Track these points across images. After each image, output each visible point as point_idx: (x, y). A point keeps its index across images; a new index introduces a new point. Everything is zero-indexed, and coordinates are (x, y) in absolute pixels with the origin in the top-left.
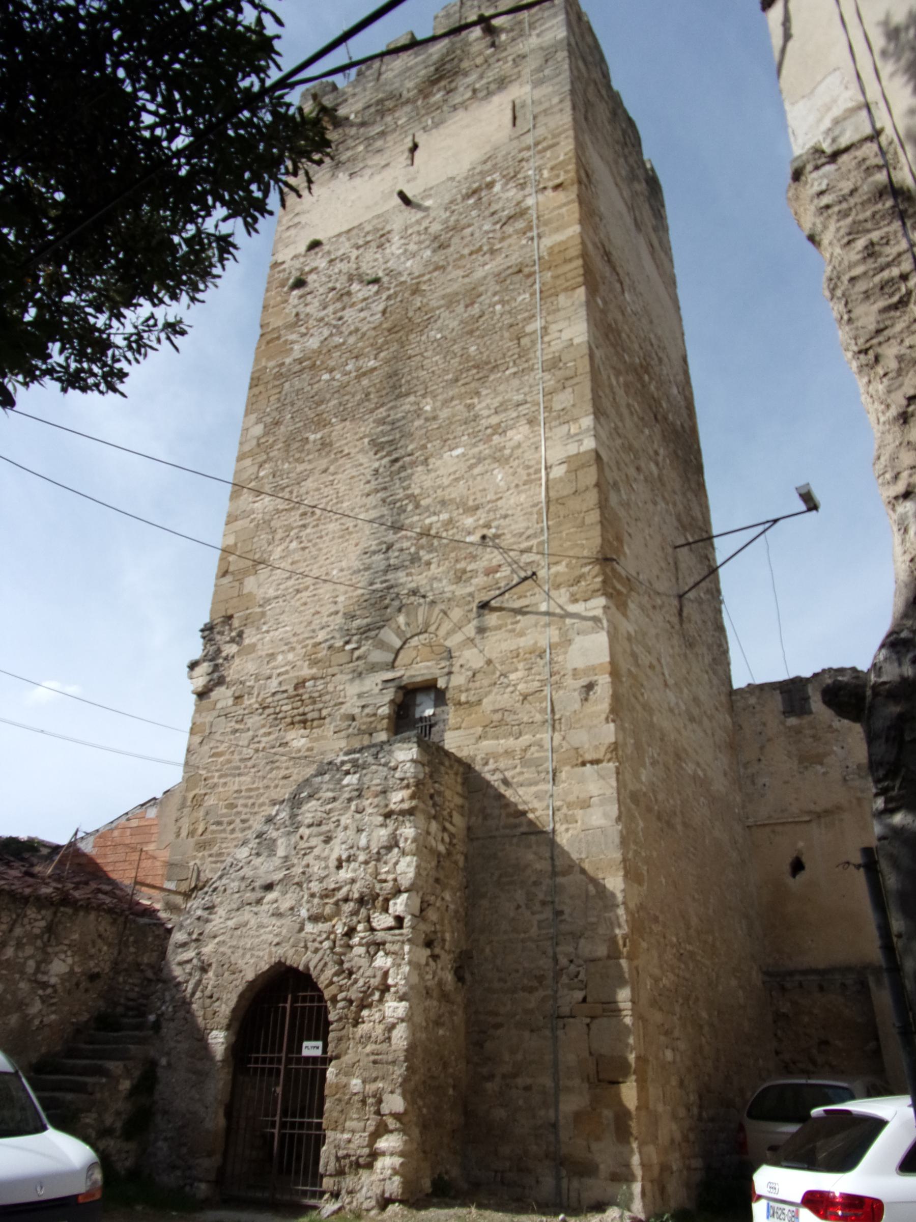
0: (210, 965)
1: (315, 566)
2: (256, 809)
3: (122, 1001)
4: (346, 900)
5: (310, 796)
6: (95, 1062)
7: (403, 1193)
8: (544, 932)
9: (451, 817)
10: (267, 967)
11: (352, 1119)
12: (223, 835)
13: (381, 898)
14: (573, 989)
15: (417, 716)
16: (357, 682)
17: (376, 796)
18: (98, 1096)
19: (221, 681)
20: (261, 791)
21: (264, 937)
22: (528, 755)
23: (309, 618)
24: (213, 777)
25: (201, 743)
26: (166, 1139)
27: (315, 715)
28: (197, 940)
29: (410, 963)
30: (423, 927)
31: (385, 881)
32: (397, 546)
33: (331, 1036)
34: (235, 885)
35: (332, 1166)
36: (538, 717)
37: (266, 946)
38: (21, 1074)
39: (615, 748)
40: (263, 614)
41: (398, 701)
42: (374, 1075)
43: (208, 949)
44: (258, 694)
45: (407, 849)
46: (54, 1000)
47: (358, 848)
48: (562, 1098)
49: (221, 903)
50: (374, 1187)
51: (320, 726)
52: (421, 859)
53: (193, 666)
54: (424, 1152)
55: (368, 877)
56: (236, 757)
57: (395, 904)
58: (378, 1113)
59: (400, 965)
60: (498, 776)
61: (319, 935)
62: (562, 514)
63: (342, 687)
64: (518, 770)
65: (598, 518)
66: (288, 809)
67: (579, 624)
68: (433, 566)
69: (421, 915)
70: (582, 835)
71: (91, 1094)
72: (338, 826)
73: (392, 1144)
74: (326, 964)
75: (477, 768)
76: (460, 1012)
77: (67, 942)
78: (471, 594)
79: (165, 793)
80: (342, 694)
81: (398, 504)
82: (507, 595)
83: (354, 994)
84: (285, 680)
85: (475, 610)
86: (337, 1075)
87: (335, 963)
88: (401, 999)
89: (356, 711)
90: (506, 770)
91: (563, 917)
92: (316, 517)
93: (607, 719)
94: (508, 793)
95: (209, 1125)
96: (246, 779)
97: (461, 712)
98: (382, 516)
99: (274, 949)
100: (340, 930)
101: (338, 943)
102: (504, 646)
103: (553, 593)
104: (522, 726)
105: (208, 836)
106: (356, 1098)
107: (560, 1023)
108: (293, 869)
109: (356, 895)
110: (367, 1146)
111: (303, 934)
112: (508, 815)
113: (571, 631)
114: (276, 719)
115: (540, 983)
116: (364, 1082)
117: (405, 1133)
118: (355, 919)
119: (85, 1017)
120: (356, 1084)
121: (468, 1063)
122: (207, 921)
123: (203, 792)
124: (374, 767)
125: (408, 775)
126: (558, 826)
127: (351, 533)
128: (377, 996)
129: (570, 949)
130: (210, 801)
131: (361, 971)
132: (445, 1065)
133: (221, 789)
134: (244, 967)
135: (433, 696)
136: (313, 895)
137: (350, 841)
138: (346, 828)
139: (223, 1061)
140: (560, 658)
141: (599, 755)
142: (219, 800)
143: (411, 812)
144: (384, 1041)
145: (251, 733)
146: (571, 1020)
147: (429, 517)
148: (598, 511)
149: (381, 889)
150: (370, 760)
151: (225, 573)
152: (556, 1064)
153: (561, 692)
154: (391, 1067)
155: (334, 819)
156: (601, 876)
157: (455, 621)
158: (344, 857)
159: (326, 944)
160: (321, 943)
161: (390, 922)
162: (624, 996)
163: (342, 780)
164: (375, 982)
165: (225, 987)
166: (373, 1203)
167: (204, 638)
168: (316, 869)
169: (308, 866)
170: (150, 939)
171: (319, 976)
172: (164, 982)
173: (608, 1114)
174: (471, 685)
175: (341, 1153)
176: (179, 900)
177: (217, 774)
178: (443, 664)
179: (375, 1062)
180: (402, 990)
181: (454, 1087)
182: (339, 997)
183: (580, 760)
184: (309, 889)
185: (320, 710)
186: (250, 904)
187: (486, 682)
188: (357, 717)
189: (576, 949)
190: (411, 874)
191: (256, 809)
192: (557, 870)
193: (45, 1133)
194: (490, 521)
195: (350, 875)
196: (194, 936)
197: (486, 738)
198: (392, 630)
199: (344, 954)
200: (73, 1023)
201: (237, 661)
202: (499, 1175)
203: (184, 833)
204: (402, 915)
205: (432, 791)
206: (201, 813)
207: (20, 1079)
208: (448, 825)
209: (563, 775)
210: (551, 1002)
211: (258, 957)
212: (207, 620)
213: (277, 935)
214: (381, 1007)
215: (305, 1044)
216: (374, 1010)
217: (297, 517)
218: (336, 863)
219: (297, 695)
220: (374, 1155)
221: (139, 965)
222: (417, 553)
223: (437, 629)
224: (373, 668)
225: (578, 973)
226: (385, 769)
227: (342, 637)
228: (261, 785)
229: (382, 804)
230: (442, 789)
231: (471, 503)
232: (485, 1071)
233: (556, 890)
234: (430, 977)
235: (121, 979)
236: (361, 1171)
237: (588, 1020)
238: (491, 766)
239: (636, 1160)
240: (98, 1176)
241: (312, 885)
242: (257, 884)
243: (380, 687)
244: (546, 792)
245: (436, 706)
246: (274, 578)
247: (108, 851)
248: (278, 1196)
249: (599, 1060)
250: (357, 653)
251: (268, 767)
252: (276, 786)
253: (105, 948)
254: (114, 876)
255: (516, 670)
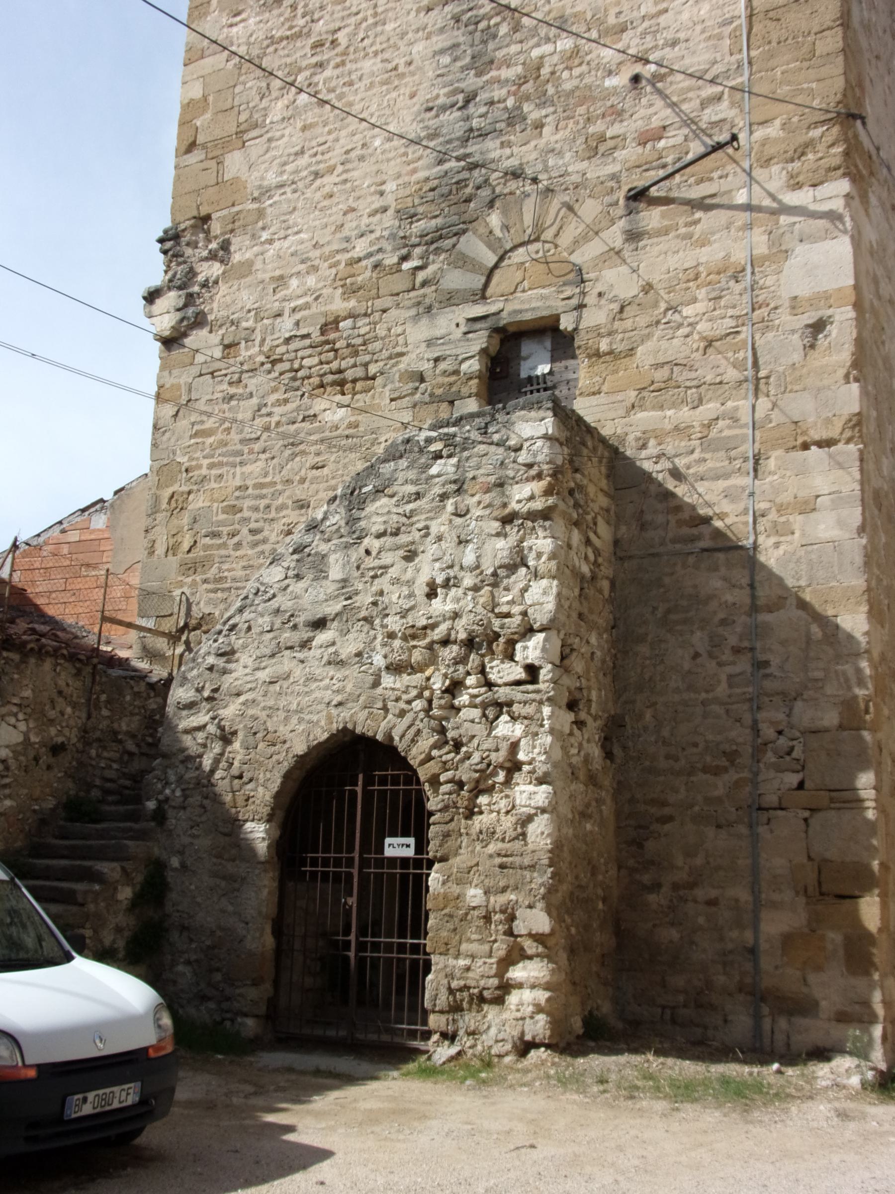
0: (235, 733)
1: (343, 133)
2: (273, 514)
3: (98, 782)
4: (445, 642)
5: (379, 491)
6: (78, 863)
7: (550, 1037)
8: (738, 691)
9: (595, 524)
10: (326, 736)
11: (469, 940)
12: (223, 552)
13: (502, 640)
14: (783, 771)
15: (524, 375)
16: (424, 321)
17: (488, 491)
18: (92, 907)
19: (199, 321)
20: (279, 487)
21: (317, 694)
22: (713, 434)
23: (339, 218)
24: (200, 467)
25: (176, 415)
26: (188, 963)
27: (359, 372)
28: (210, 699)
29: (552, 731)
30: (566, 681)
31: (508, 615)
32: (483, 96)
33: (433, 831)
34: (265, 621)
35: (443, 1000)
36: (732, 374)
37: (320, 707)
38: (17, 880)
39: (857, 422)
40: (261, 213)
41: (493, 351)
42: (502, 884)
43: (230, 711)
44: (263, 340)
45: (542, 569)
46: (7, 781)
47: (462, 568)
48: (764, 915)
49: (244, 646)
50: (507, 1027)
51: (366, 391)
52: (561, 584)
53: (151, 297)
54: (574, 984)
55: (479, 609)
56: (235, 437)
57: (525, 648)
58: (510, 933)
59: (537, 734)
60: (665, 464)
61: (405, 692)
62: (774, 37)
63: (399, 330)
64: (696, 455)
65: (840, 45)
66: (342, 510)
67: (802, 224)
68: (546, 130)
69: (563, 662)
70: (802, 552)
71: (82, 905)
72: (427, 535)
73: (534, 974)
74: (419, 732)
75: (628, 453)
76: (609, 801)
77: (16, 700)
78: (614, 177)
79: (116, 493)
80: (401, 340)
81: (482, 25)
82: (678, 178)
83: (465, 774)
84: (305, 319)
85: (622, 202)
86: (444, 883)
87: (433, 730)
88: (541, 781)
89: (426, 366)
90: (676, 456)
91: (768, 671)
92: (339, 50)
93: (847, 377)
94: (680, 490)
95: (251, 945)
96: (256, 468)
97: (600, 367)
98: (456, 46)
99: (334, 712)
100: (438, 684)
101: (435, 703)
102: (673, 262)
103: (757, 173)
104: (703, 389)
105: (198, 553)
106: (476, 913)
107: (764, 816)
108: (355, 598)
109: (462, 636)
110: (495, 976)
111: (379, 690)
112: (680, 523)
113: (787, 236)
114: (294, 379)
115: (732, 762)
116: (487, 893)
117: (550, 959)
118: (461, 668)
119: (50, 803)
120: (474, 895)
121: (620, 868)
122: (225, 672)
123: (185, 489)
124: (482, 447)
125: (540, 458)
126: (761, 539)
127: (402, 76)
128: (501, 776)
129: (781, 716)
130: (198, 502)
131: (475, 742)
132: (594, 871)
133: (213, 485)
134: (289, 736)
135: (548, 344)
136: (391, 636)
137: (447, 558)
138: (440, 539)
139: (877, 886)
140: (770, 281)
141: (833, 432)
142: (213, 500)
143: (545, 515)
144: (516, 838)
145: (255, 401)
146: (780, 813)
147: (538, 45)
148: (839, 31)
149: (502, 627)
150: (475, 435)
151: (191, 147)
152: (755, 870)
153: (770, 335)
154: (527, 874)
155: (420, 525)
156: (830, 612)
157: (589, 221)
158: (439, 580)
159: (418, 705)
160: (409, 702)
161: (519, 673)
162: (865, 781)
163: (429, 466)
164: (498, 757)
165: (261, 764)
166: (508, 1047)
167: (165, 252)
168: (394, 598)
169: (381, 593)
170: (128, 698)
171: (408, 749)
172: (165, 756)
173: (834, 937)
174: (617, 324)
175: (455, 984)
176: (161, 644)
177: (206, 462)
178: (568, 292)
179: (502, 866)
180: (541, 769)
181: (604, 900)
182: (442, 778)
183: (800, 440)
184: (383, 626)
185: (366, 365)
186: (291, 648)
187: (642, 321)
188: (428, 375)
189: (788, 716)
190: (550, 604)
191: (273, 514)
192: (760, 602)
193: (73, 963)
194: (647, 51)
195: (449, 607)
196: (206, 694)
197: (642, 408)
198: (480, 237)
199: (447, 719)
200: (34, 811)
201: (223, 288)
202: (668, 1012)
203: (160, 549)
204: (537, 663)
205: (572, 485)
206: (185, 520)
207: (20, 889)
208: (592, 536)
209: (772, 463)
210: (748, 789)
211: (309, 722)
212: (168, 224)
213: (338, 691)
214: (507, 792)
215: (388, 841)
216: (496, 796)
217: (308, 50)
218: (426, 589)
219: (327, 342)
220: (506, 987)
221: (115, 733)
222: (519, 108)
223: (556, 235)
224: (451, 299)
225: (792, 749)
226: (501, 450)
227: (395, 249)
228: (277, 479)
229: (498, 502)
230: (585, 482)
231: (612, 20)
232: (646, 878)
233: (759, 631)
234: (574, 751)
235: (93, 752)
236: (486, 1007)
237: (807, 814)
238: (652, 449)
239: (877, 997)
240: (167, 1021)
241: (389, 620)
242: (301, 620)
243: (463, 328)
244: (743, 489)
245: (553, 360)
246: (273, 153)
247: (37, 575)
248: (360, 1036)
249: (822, 866)
250: (421, 276)
251: (288, 452)
252: (303, 481)
253: (69, 710)
254: (51, 611)
255: (695, 300)
